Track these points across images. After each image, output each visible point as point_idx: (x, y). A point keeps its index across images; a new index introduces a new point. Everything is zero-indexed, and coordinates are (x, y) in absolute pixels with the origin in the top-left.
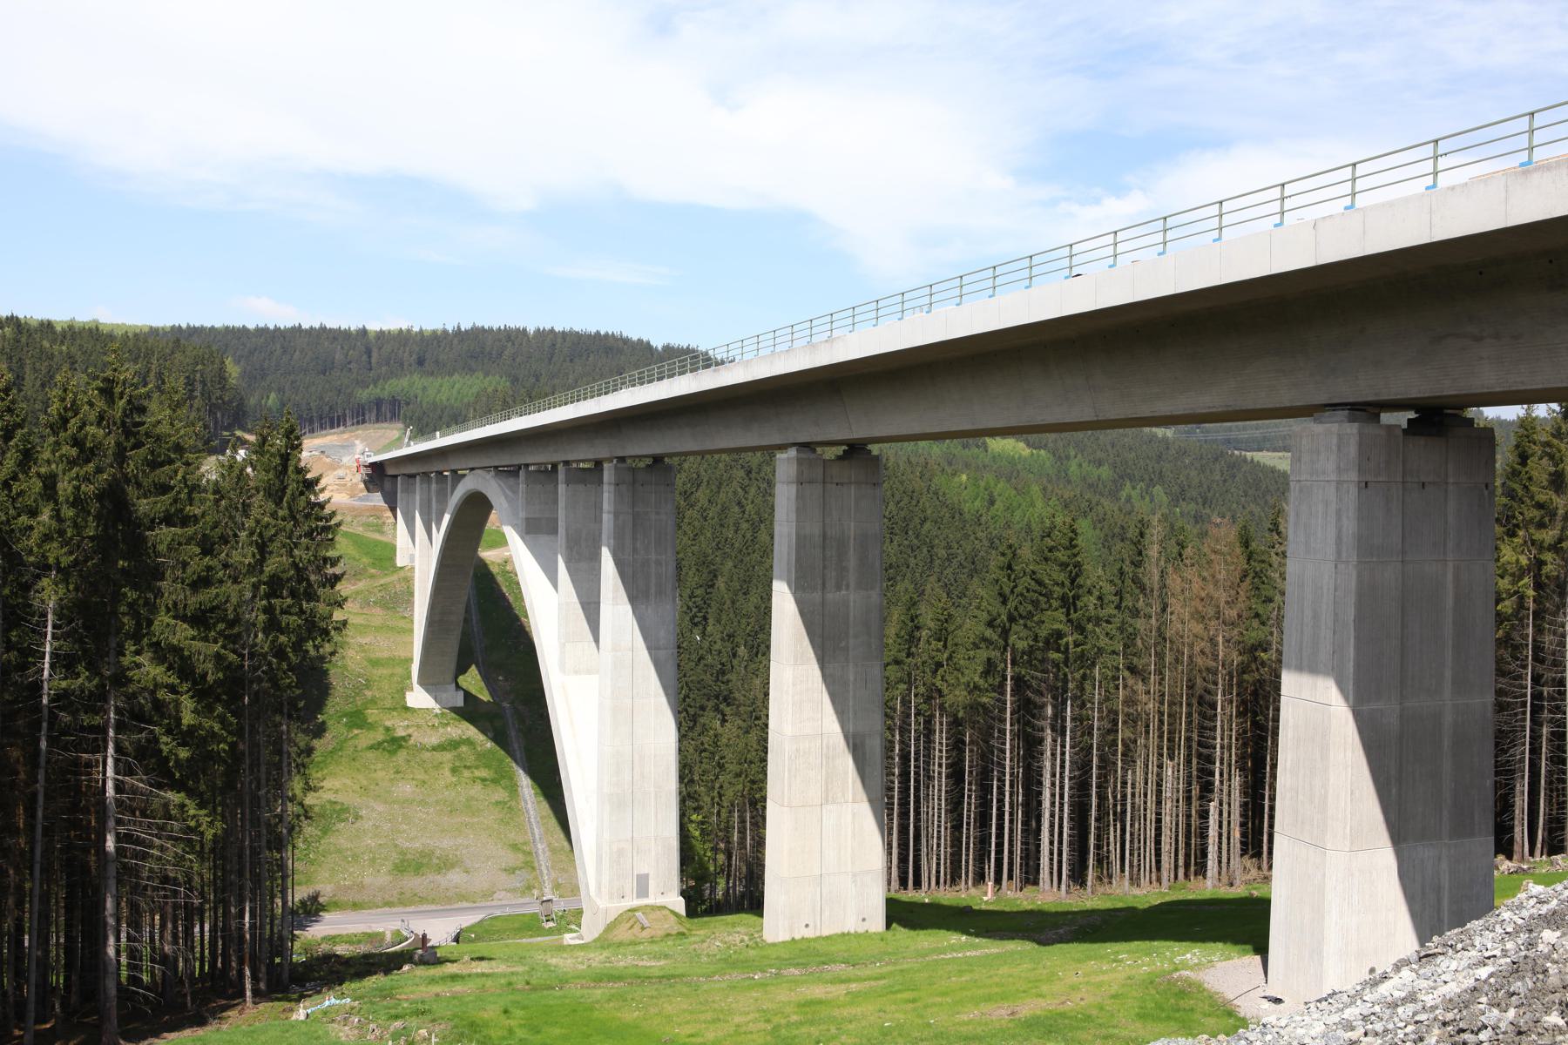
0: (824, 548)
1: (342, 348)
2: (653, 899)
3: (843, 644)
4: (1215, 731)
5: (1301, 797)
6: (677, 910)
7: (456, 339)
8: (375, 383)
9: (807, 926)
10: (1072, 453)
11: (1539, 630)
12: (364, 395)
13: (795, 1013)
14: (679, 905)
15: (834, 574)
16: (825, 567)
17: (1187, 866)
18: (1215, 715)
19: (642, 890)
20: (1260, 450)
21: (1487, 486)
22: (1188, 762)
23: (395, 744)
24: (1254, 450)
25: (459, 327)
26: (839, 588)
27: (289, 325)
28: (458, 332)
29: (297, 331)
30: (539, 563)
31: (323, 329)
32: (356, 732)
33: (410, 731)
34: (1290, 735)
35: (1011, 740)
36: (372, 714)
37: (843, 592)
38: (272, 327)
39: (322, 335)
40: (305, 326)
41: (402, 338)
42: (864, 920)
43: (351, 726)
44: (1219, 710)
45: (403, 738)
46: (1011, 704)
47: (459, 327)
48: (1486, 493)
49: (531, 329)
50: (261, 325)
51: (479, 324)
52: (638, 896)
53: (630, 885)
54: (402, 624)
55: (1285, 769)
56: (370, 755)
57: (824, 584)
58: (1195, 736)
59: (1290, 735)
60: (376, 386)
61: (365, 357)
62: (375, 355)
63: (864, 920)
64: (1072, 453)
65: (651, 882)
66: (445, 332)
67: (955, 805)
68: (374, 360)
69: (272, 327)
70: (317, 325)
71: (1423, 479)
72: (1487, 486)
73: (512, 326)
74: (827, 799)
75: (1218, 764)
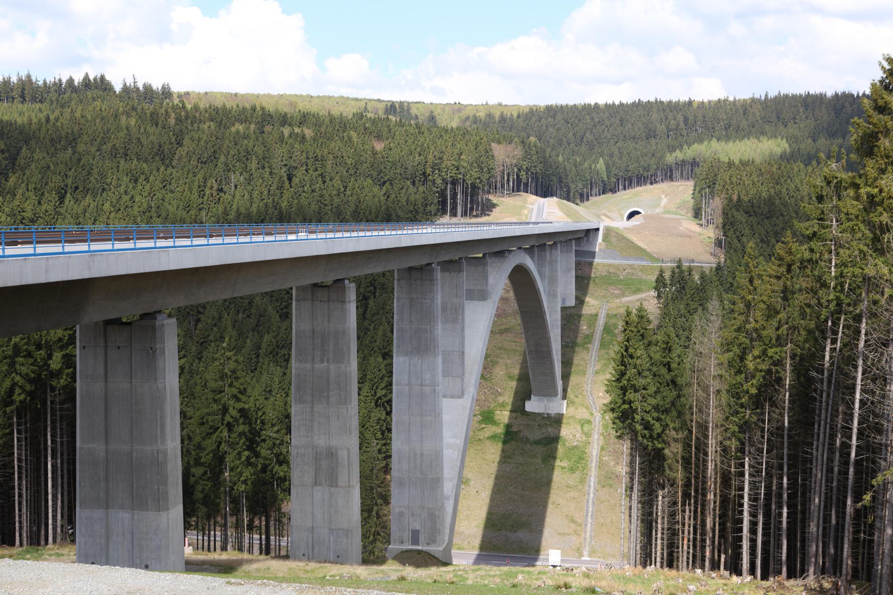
0: (313, 339)
3: (325, 394)
11: (488, 418)
12: (671, 158)
15: (319, 353)
16: (314, 349)
17: (693, 562)
21: (152, 348)
26: (322, 362)
32: (483, 426)
37: (325, 364)
42: (338, 557)
45: (516, 433)
48: (151, 351)
52: (413, 544)
56: (488, 443)
57: (313, 359)
63: (338, 557)
70: (652, 99)
71: (118, 344)
72: (152, 348)
74: (316, 483)
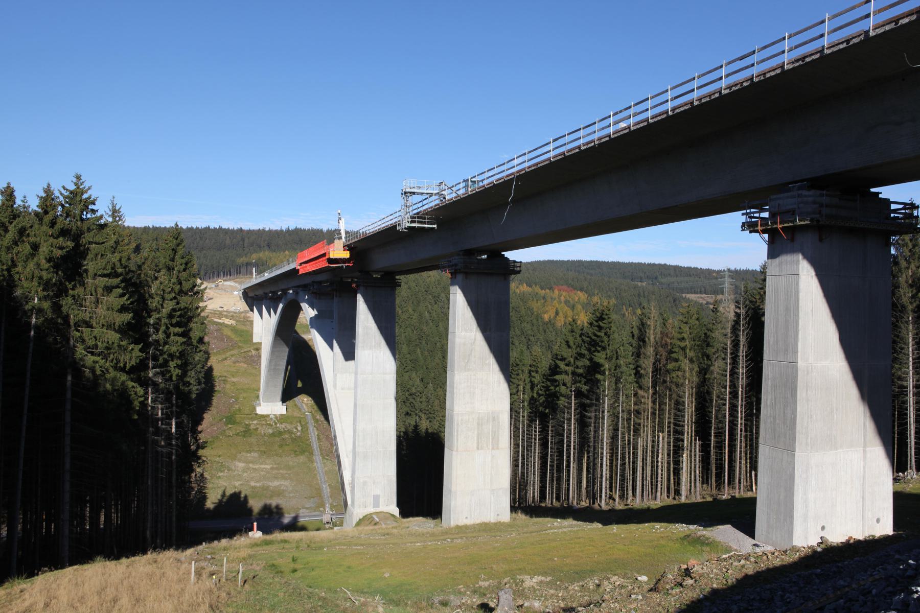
1: (230, 238)
2: (383, 508)
3: (487, 362)
4: (684, 417)
5: (777, 421)
6: (395, 514)
7: (287, 234)
8: (246, 255)
9: (466, 518)
10: (596, 292)
13: (520, 291)
14: (396, 511)
18: (685, 409)
19: (376, 504)
20: (688, 293)
22: (669, 435)
23: (247, 432)
24: (686, 293)
25: (288, 228)
27: (204, 226)
28: (288, 230)
29: (207, 229)
30: (322, 337)
31: (220, 228)
32: (230, 426)
33: (258, 426)
34: (770, 383)
35: (574, 424)
36: (238, 418)
38: (195, 227)
39: (220, 231)
40: (212, 227)
41: (260, 233)
43: (226, 424)
44: (686, 406)
46: (575, 405)
47: (288, 228)
49: (325, 229)
50: (190, 226)
51: (299, 227)
53: (370, 500)
54: (254, 371)
55: (767, 405)
58: (672, 420)
59: (770, 383)
60: (246, 257)
61: (241, 243)
62: (246, 241)
64: (596, 292)
65: (381, 500)
66: (282, 231)
67: (544, 458)
68: (245, 245)
69: (195, 227)
73: (315, 228)
75: (686, 435)
